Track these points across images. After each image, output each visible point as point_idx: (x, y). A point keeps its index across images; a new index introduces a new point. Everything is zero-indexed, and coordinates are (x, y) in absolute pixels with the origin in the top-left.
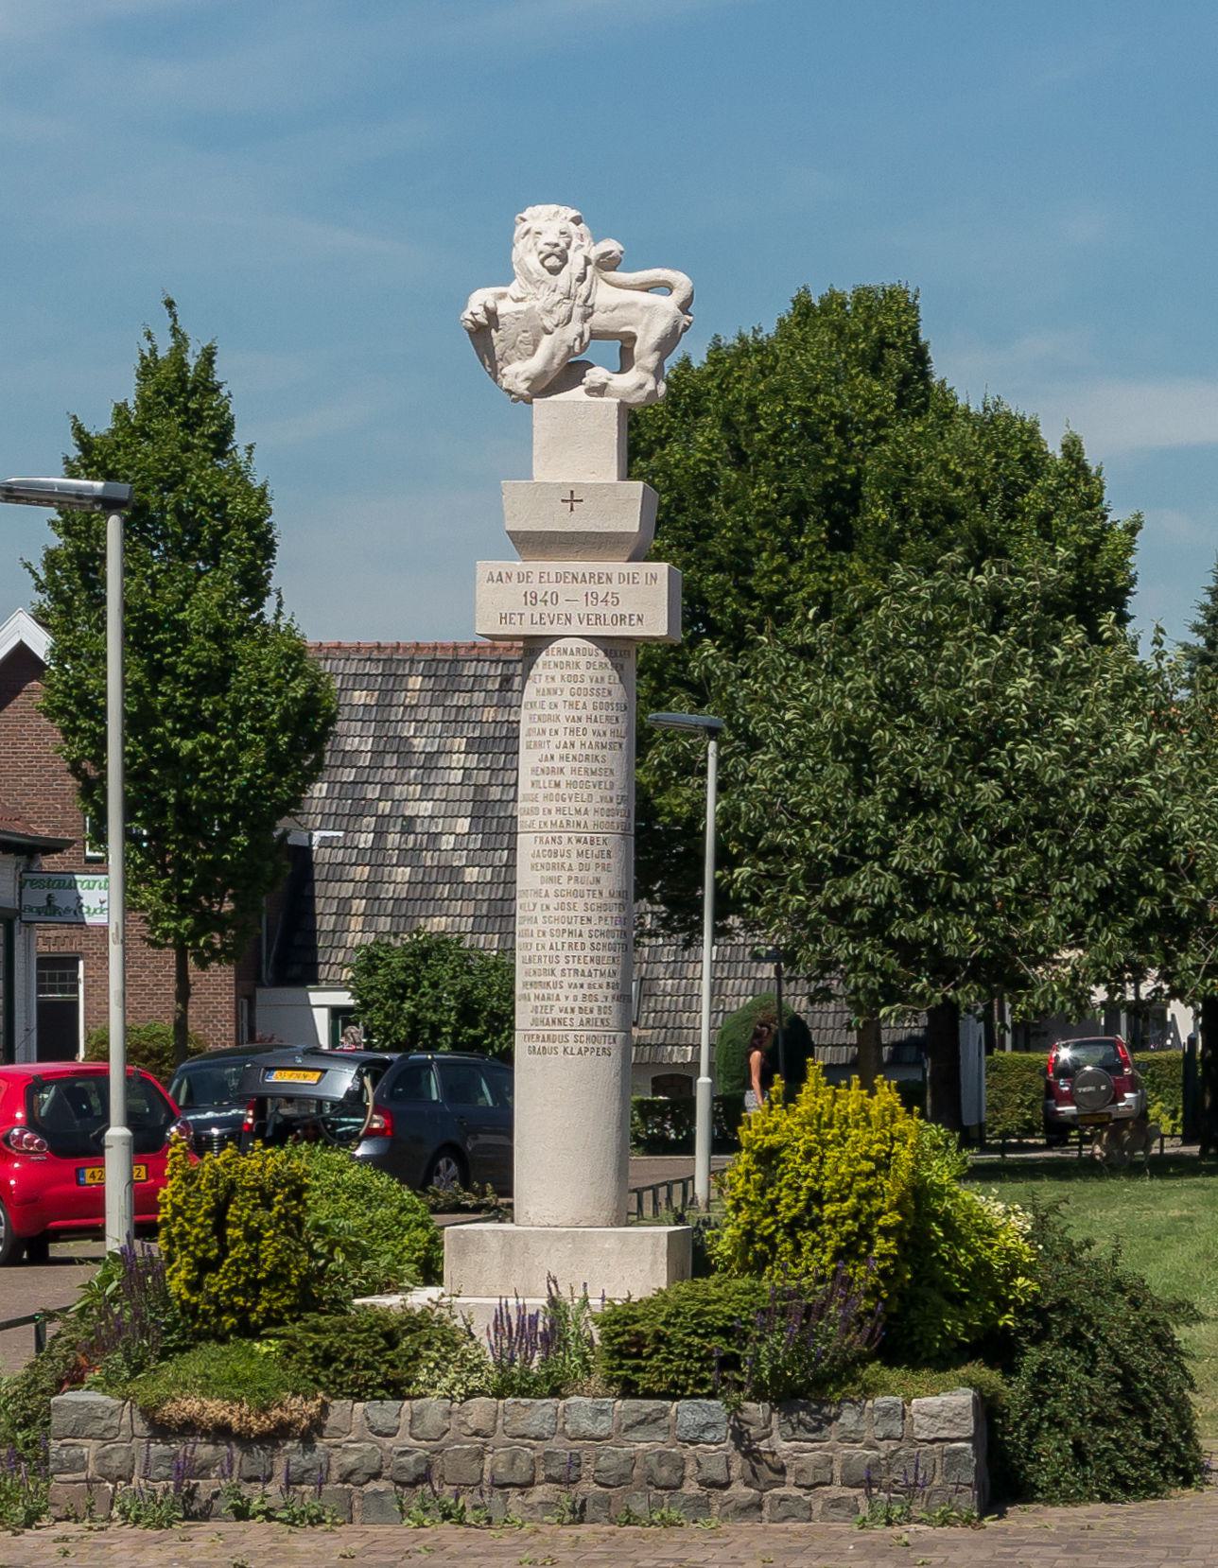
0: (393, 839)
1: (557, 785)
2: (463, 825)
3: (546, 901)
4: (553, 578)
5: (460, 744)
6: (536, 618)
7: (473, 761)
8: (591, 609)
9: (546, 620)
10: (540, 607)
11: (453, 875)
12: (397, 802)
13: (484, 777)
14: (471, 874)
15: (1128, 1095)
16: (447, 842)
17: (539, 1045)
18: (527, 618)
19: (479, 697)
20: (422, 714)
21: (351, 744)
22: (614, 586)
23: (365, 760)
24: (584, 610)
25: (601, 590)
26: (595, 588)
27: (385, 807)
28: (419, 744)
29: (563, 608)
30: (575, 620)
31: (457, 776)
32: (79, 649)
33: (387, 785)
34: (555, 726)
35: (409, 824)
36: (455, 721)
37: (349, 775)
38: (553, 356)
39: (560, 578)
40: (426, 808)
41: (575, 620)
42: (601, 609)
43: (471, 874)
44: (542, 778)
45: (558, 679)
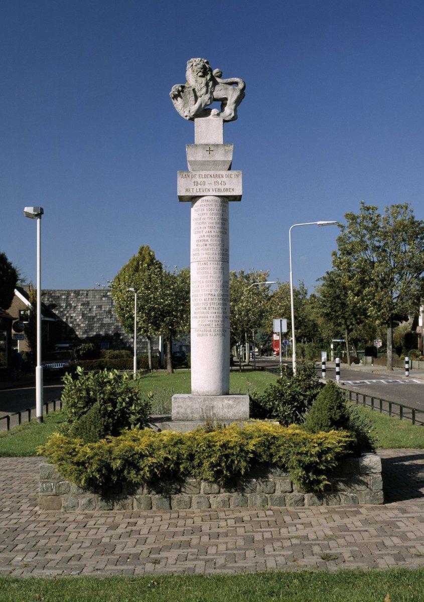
0: (69, 320)
1: (206, 245)
2: (81, 317)
3: (202, 284)
4: (203, 176)
5: (80, 304)
6: (198, 190)
7: (82, 307)
8: (217, 187)
9: (201, 190)
10: (199, 186)
11: (79, 325)
12: (70, 314)
13: (84, 310)
14: (82, 325)
15: (82, 344)
16: (78, 320)
17: (201, 333)
18: (195, 191)
19: (83, 297)
20: (73, 300)
21: (62, 305)
22: (224, 179)
23: (64, 307)
24: (214, 187)
25: (219, 180)
26: (218, 179)
27: (68, 315)
28: (73, 305)
29: (207, 186)
30: (211, 190)
31: (79, 310)
32: (105, 517)
33: (68, 311)
34: (205, 225)
35: (72, 317)
36: (78, 301)
37: (62, 310)
38: (201, 105)
39: (206, 176)
40: (74, 315)
41: (211, 190)
42: (220, 187)
43: (82, 325)
44: (200, 243)
45: (205, 210)
